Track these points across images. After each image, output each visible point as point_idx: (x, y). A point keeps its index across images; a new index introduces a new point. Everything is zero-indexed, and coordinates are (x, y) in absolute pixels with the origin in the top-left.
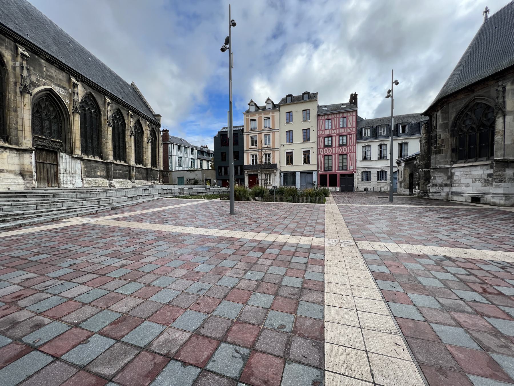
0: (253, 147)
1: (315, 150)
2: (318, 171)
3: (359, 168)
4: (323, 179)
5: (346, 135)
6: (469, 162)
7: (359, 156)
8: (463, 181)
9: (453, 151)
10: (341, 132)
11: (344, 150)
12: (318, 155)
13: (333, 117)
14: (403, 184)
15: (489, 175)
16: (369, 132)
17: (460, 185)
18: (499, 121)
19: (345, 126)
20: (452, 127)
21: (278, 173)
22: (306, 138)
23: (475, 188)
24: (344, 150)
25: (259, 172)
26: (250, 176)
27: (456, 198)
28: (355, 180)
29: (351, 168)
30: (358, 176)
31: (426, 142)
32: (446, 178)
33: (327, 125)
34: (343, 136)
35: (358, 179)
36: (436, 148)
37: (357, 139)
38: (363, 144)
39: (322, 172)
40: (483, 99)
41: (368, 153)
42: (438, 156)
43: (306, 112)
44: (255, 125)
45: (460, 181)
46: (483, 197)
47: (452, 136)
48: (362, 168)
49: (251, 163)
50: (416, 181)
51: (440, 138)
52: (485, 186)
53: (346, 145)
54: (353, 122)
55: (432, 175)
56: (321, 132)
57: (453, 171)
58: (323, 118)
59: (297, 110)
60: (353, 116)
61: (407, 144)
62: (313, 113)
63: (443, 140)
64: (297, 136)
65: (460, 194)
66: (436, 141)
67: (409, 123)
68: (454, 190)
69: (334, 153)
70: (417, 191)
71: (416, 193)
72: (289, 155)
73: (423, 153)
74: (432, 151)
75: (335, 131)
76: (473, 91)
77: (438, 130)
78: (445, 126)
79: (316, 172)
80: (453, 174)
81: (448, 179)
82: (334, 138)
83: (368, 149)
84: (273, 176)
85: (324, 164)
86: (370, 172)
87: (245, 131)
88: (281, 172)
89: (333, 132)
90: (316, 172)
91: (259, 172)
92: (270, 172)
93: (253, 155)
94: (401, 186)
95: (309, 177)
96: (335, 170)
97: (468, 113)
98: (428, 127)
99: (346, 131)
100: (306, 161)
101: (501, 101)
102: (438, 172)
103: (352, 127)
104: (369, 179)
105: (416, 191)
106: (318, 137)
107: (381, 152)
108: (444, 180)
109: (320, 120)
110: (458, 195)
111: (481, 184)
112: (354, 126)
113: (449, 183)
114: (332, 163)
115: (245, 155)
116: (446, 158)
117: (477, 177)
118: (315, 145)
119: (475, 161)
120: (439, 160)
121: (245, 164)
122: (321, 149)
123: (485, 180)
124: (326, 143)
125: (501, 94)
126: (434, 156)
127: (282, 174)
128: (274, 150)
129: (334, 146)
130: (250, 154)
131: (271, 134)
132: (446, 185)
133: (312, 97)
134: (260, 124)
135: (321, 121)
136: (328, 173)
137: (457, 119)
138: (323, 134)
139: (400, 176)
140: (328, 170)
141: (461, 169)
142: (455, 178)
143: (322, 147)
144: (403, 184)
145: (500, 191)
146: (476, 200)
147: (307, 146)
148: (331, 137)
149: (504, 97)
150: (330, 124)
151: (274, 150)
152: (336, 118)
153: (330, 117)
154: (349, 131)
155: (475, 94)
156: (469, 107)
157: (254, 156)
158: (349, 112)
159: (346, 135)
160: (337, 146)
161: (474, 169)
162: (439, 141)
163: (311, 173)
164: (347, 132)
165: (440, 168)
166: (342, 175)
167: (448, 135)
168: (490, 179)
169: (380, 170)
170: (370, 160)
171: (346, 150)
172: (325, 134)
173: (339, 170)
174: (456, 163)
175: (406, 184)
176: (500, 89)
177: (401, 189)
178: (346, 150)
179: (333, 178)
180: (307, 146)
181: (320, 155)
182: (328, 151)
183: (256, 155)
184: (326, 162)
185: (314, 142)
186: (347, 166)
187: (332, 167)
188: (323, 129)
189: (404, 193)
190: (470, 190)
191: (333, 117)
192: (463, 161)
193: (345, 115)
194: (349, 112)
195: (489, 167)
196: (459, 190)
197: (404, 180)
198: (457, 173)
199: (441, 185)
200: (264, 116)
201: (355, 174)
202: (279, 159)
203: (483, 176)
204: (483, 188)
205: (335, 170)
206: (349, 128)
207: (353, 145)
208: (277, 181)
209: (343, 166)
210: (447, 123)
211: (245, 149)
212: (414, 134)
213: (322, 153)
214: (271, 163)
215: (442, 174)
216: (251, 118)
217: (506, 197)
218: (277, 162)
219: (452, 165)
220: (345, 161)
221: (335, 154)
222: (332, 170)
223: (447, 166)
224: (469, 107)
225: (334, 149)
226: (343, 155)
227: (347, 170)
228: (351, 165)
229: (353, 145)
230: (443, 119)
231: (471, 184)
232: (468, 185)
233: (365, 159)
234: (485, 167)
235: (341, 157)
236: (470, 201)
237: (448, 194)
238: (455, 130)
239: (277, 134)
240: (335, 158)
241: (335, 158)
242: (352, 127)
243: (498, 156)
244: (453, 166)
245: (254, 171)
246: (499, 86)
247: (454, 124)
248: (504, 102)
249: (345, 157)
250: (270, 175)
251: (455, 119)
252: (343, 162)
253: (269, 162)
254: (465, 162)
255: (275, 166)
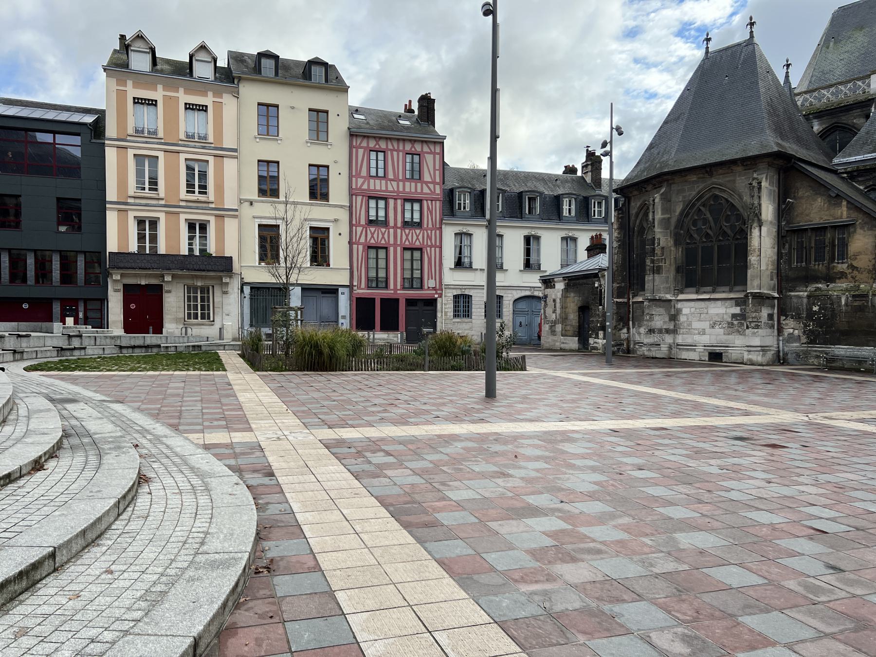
0: (191, 197)
1: (345, 229)
2: (350, 287)
3: (448, 287)
4: (364, 313)
5: (420, 201)
6: (705, 292)
7: (449, 259)
8: (696, 325)
9: (678, 270)
10: (407, 189)
11: (415, 237)
12: (351, 243)
13: (390, 147)
14: (559, 328)
15: (734, 316)
16: (467, 202)
17: (689, 332)
18: (755, 232)
19: (416, 176)
20: (676, 227)
21: (234, 286)
22: (318, 190)
23: (713, 337)
24: (415, 237)
25: (168, 278)
26: (130, 293)
27: (685, 355)
28: (439, 315)
29: (432, 283)
30: (445, 306)
31: (619, 247)
32: (667, 319)
33: (373, 164)
34: (412, 201)
35: (446, 313)
36: (653, 261)
37: (443, 215)
38: (457, 229)
39: (362, 291)
40: (725, 191)
41: (466, 252)
42: (657, 276)
43: (319, 116)
44: (145, 118)
45: (690, 324)
46: (726, 352)
47: (677, 243)
48: (456, 287)
49: (133, 247)
50: (596, 320)
51: (659, 244)
52: (729, 334)
53: (419, 225)
54: (435, 169)
55: (646, 311)
56: (360, 181)
57: (679, 305)
58: (364, 144)
59: (293, 104)
60: (434, 154)
61: (537, 238)
62: (338, 127)
63: (663, 248)
64: (295, 182)
65: (691, 347)
66: (654, 249)
67: (541, 194)
68: (680, 339)
69: (392, 242)
70: (600, 341)
71: (600, 346)
72: (268, 234)
73: (615, 268)
74: (648, 268)
75: (395, 184)
76: (711, 174)
77: (657, 229)
78: (665, 223)
79: (346, 290)
80: (679, 312)
81: (670, 320)
82: (391, 202)
83: (466, 241)
84: (217, 296)
85: (367, 269)
86: (469, 297)
87: (111, 129)
88: (243, 284)
89: (390, 188)
90: (346, 290)
91: (168, 278)
92: (208, 283)
93: (141, 222)
94: (553, 332)
95: (325, 303)
96: (395, 289)
97: (702, 208)
98: (621, 218)
99: (419, 190)
100: (320, 255)
101: (756, 202)
102: (656, 306)
103: (434, 182)
104: (468, 314)
105: (599, 342)
106: (352, 194)
107: (460, 253)
108: (665, 322)
109: (357, 148)
110: (688, 350)
111: (722, 330)
112: (438, 180)
113: (672, 327)
114: (387, 268)
115: (112, 218)
116: (667, 282)
117: (717, 319)
118: (344, 216)
119: (714, 292)
120: (659, 284)
121: (112, 245)
122: (359, 229)
123: (729, 323)
124: (372, 213)
125: (756, 190)
126: (651, 278)
127: (247, 290)
128: (222, 213)
129: (392, 224)
130: (131, 215)
131: (211, 159)
132: (668, 331)
133: (317, 75)
134: (171, 121)
135: (361, 151)
136: (378, 294)
137: (684, 214)
138: (365, 187)
139: (549, 310)
140: (377, 287)
141: (692, 304)
142: (682, 319)
143: (363, 222)
144: (559, 328)
145: (756, 342)
146: (716, 357)
147: (320, 214)
148: (385, 199)
149: (760, 197)
150: (381, 164)
151: (222, 213)
152: (398, 151)
153: (383, 145)
154: (426, 190)
155: (714, 180)
156: (703, 200)
157: (147, 227)
158: (426, 142)
159: (420, 201)
160: (399, 224)
161: (712, 304)
162: (658, 251)
163: (331, 291)
164: (422, 193)
165: (660, 300)
166: (410, 302)
167: (671, 242)
168: (735, 322)
169: (459, 292)
170: (470, 267)
171: (420, 237)
172: (369, 190)
173: (403, 288)
174: (682, 293)
175: (568, 328)
176: (755, 184)
177: (555, 338)
178: (420, 237)
179: (390, 305)
180: (320, 214)
181: (358, 244)
182: (377, 236)
183: (154, 223)
184: (372, 263)
185: (342, 207)
186: (422, 279)
187: (387, 279)
188: (364, 173)
189: (563, 346)
190: (705, 339)
191: (390, 147)
192: (694, 289)
193: (418, 147)
194: (426, 142)
195: (734, 302)
196: (689, 340)
197: (564, 319)
198: (685, 311)
199: (660, 331)
200: (184, 98)
201: (439, 300)
202: (237, 242)
203: (725, 317)
204: (726, 337)
205: (395, 289)
206: (427, 183)
207: (434, 228)
208: (231, 314)
209: (412, 278)
210: (669, 219)
211: (111, 194)
212: (549, 219)
213: (362, 240)
214: (162, 249)
215: (662, 310)
216: (133, 92)
217: (763, 351)
218: (230, 251)
219: (678, 295)
220: (416, 265)
221: (395, 245)
222: (387, 287)
223: (669, 297)
224: (703, 200)
225: (392, 231)
226: (412, 249)
227: (421, 287)
228: (430, 276)
229: (434, 228)
230: (665, 210)
231: (708, 331)
232: (703, 332)
233: (459, 264)
234: (728, 303)
235: (408, 255)
236: (707, 359)
237: (670, 348)
238: (681, 232)
239: (230, 165)
240: (396, 255)
241: (396, 255)
242: (434, 182)
243: (753, 288)
244: (679, 298)
245: (150, 276)
246: (754, 179)
247: (680, 224)
248: (760, 205)
249: (382, 254)
250: (205, 290)
251: (681, 213)
252: (412, 269)
253: (154, 249)
254: (697, 293)
255: (225, 265)
